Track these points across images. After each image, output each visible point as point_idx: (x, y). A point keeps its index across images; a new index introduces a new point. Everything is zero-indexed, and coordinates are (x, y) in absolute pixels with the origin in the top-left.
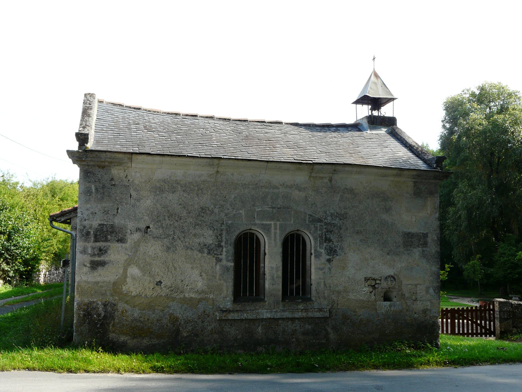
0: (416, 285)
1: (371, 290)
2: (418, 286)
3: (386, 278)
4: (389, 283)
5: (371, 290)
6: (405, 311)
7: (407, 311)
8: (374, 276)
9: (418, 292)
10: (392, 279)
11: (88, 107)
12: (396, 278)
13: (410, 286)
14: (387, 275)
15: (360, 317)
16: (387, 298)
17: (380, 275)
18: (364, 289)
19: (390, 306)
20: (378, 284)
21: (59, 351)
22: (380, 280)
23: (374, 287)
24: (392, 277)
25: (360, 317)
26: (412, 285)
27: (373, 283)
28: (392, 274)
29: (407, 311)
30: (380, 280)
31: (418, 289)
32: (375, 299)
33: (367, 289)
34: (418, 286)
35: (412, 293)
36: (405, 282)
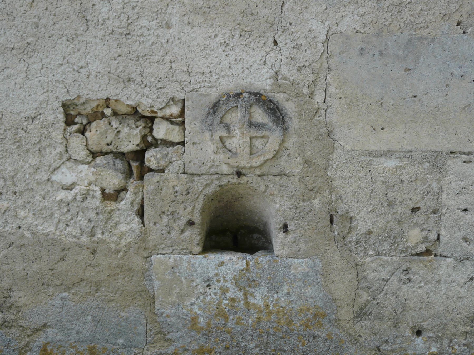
0: (437, 161)
1: (113, 180)
2: (455, 165)
3: (216, 106)
4: (238, 141)
5: (113, 180)
6: (345, 315)
7: (360, 314)
8: (127, 98)
9: (450, 201)
10: (259, 115)
11: (166, 23)
12: (289, 107)
13: (391, 163)
14: (228, 85)
15: (40, 339)
16: (232, 230)
17: (173, 90)
18: (66, 175)
19: (246, 283)
20: (167, 143)
21: (274, 243)
22: (179, 121)
23: (135, 163)
24: (258, 98)
25: (40, 339)
26: (406, 154)
27: (130, 139)
28: (262, 81)
29: (360, 314)
30: (179, 121)
31: (452, 182)
32: (143, 235)
33: (81, 175)
34: (455, 165)
35: (402, 211)
36: (352, 137)
